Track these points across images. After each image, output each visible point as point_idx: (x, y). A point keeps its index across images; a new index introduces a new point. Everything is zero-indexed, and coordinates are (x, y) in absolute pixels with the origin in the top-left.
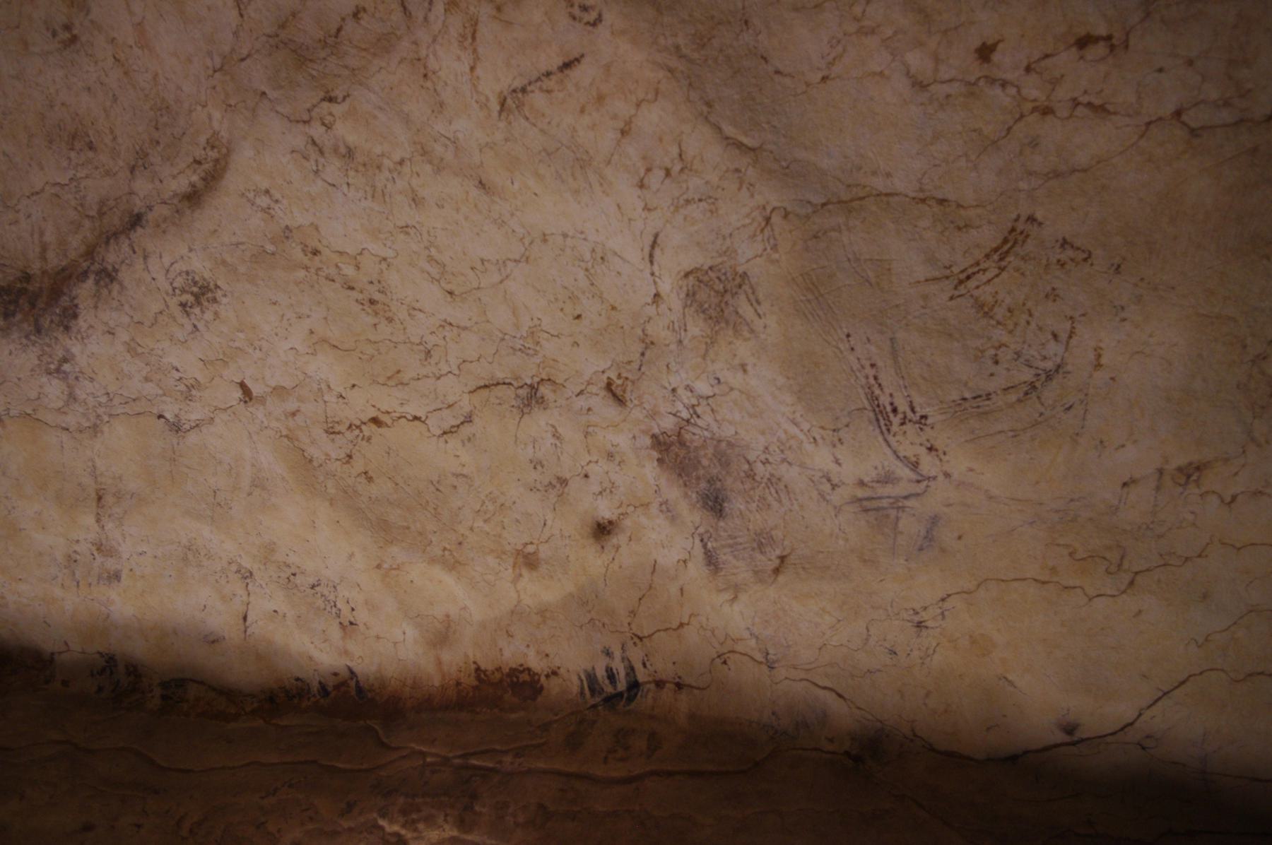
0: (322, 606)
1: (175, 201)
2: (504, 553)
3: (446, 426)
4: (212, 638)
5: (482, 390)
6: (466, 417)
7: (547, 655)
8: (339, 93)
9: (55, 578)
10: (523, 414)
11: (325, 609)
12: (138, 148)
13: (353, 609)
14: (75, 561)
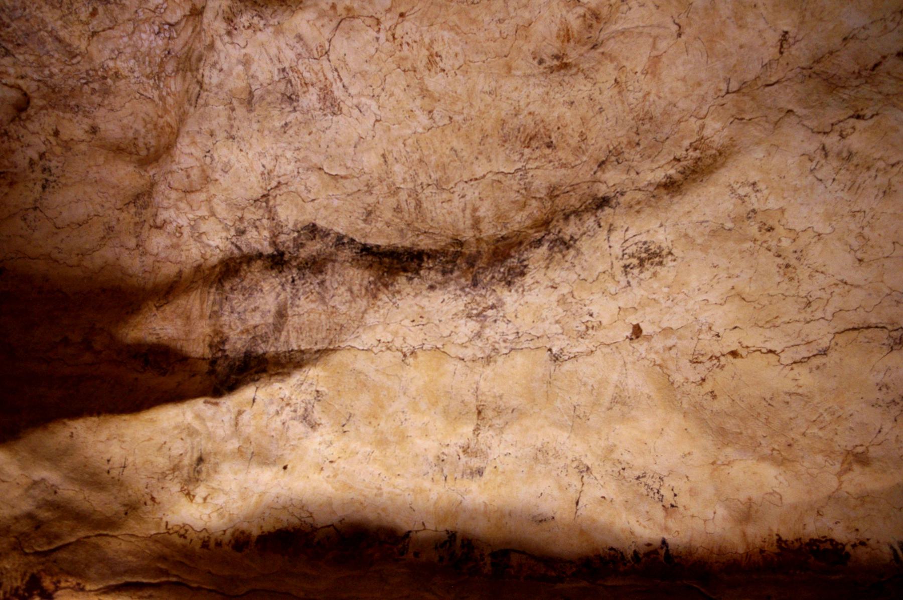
0: (645, 493)
1: (651, 189)
2: (832, 452)
3: (798, 357)
4: (540, 518)
5: (851, 332)
6: (820, 351)
7: (857, 530)
8: (868, 113)
9: (426, 474)
10: (892, 350)
11: (648, 495)
12: (611, 147)
13: (675, 495)
14: (443, 460)
